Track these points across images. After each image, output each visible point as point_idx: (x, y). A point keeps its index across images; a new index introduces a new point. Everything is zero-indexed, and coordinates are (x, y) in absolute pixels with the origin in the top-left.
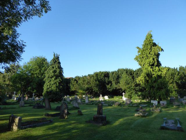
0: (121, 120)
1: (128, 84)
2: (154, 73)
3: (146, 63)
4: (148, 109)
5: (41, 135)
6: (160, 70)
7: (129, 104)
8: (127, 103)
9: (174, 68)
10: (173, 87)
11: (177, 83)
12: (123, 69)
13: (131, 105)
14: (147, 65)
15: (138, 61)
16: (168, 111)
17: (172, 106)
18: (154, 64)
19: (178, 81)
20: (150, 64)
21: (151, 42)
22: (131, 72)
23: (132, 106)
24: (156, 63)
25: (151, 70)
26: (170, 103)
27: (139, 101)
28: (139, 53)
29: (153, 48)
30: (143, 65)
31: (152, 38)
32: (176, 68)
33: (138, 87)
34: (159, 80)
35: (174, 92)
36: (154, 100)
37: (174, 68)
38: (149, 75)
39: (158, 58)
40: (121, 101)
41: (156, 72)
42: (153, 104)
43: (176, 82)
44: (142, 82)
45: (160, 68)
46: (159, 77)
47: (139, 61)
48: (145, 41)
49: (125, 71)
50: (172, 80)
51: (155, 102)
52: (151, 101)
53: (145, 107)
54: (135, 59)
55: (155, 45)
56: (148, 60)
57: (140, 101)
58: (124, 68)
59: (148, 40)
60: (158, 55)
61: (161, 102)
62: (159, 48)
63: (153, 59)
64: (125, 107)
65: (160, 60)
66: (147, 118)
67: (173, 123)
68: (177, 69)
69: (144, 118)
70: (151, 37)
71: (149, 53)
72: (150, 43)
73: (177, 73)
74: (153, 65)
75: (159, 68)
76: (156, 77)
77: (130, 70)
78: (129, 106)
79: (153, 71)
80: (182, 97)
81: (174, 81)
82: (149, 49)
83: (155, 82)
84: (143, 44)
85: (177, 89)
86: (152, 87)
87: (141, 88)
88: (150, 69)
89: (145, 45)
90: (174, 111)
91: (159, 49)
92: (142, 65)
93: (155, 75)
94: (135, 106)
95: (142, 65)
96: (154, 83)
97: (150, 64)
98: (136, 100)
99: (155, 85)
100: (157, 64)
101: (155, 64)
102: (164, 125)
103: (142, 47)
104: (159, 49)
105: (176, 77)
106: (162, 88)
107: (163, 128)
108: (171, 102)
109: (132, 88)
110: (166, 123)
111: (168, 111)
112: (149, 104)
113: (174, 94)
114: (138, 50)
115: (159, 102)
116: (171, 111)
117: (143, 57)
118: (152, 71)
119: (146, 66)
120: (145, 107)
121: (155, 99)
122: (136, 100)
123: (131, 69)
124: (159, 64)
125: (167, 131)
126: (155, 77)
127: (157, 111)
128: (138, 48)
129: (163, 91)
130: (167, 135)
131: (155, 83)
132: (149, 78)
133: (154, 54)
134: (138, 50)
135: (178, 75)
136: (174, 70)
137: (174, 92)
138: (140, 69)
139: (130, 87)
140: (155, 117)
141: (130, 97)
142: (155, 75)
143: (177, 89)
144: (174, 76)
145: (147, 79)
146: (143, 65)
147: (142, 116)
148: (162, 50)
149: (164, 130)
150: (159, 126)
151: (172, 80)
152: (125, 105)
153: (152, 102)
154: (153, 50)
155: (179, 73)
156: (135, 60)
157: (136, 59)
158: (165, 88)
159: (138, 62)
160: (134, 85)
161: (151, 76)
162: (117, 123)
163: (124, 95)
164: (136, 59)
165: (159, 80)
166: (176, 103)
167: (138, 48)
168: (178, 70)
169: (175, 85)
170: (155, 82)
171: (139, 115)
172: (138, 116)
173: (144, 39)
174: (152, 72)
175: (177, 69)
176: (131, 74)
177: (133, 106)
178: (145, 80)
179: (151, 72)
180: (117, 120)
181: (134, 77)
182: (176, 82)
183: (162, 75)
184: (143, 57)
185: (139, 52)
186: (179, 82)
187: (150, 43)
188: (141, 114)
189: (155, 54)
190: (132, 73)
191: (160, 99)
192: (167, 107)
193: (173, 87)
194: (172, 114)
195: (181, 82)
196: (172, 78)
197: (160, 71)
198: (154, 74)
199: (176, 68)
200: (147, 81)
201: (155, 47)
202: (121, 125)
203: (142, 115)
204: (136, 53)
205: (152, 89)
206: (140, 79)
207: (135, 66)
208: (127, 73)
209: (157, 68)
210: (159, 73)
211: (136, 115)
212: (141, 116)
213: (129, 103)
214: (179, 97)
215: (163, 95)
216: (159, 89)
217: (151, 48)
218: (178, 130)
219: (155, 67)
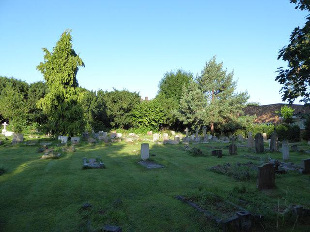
0: (24, 165)
1: (18, 108)
2: (68, 96)
3: (58, 78)
4: (56, 149)
5: (132, 156)
6: (76, 92)
7: (20, 142)
8: (14, 141)
9: (92, 91)
10: (88, 116)
11: (93, 113)
12: (5, 78)
13: (25, 144)
14: (59, 82)
15: (43, 72)
16: (83, 150)
17: (87, 144)
18: (69, 82)
19: (94, 110)
20: (62, 81)
21: (69, 48)
22: (22, 87)
23: (27, 146)
24: (72, 81)
25: (64, 90)
26: (84, 139)
27: (37, 137)
28: (47, 60)
29: (71, 57)
30: (52, 82)
31: (71, 42)
32: (93, 91)
33: (33, 114)
34: (74, 108)
35: (88, 125)
36: (62, 136)
37: (92, 91)
38: (59, 98)
39: (76, 75)
40: (3, 138)
41: (70, 95)
42: (60, 141)
43: (92, 111)
44: (47, 108)
45: (77, 90)
46: (74, 102)
47: (46, 74)
48: (59, 42)
49: (11, 84)
50: (87, 107)
51: (63, 139)
52: (58, 137)
53: (51, 145)
54: (37, 67)
55: (73, 53)
56: (60, 75)
57: (38, 138)
58: (9, 76)
59: (65, 43)
60: (76, 70)
61: (73, 138)
62: (79, 60)
63: (69, 75)
64: (13, 147)
65: (77, 77)
66: (60, 159)
67: (94, 162)
68: (95, 92)
69: (56, 160)
70: (70, 39)
71: (64, 65)
72: (67, 48)
73: (94, 99)
74: (67, 84)
75: (75, 89)
76: (69, 102)
77: (20, 81)
78: (21, 146)
79: (66, 92)
80: (96, 132)
81: (89, 109)
82: (64, 58)
83: (67, 109)
84: (55, 46)
85: (91, 120)
86: (62, 116)
87: (38, 115)
88: (61, 88)
89: (59, 50)
90: (90, 150)
91: (79, 62)
92: (50, 81)
93: (68, 100)
94: (31, 146)
95: (50, 81)
96: (66, 110)
97: (62, 81)
98: (32, 134)
99: (66, 113)
100: (74, 83)
101: (70, 83)
102: (86, 164)
103: (53, 52)
104: (79, 62)
105: (93, 104)
106: (76, 119)
107: (86, 168)
108: (84, 138)
109: (24, 116)
110: (87, 162)
111: (83, 150)
112: (54, 141)
113: (88, 127)
114: (45, 53)
115: (69, 139)
116: (87, 150)
117: (53, 69)
118: (65, 92)
119: (57, 83)
120: (51, 145)
121: (64, 134)
122: (30, 136)
123: (23, 80)
124: (75, 84)
125: (90, 170)
126: (68, 102)
127: (70, 150)
128: (45, 50)
129: (77, 123)
130: (92, 173)
131: (67, 111)
132: (59, 102)
133: (71, 68)
134: (45, 53)
135: (96, 101)
136: (92, 93)
137: (88, 125)
138: (39, 84)
139: (20, 114)
140: (71, 158)
141: (19, 130)
142: (68, 100)
143: (91, 120)
144: (90, 103)
145: (56, 102)
146: (52, 82)
147: (54, 158)
148: (83, 64)
149: (88, 170)
150: (81, 167)
151: (87, 107)
152: (11, 143)
153: (59, 138)
154: (70, 61)
155: (97, 99)
156: (38, 69)
157: (41, 68)
158: (80, 118)
159: (43, 74)
160: (28, 110)
161: (63, 101)
162: (21, 169)
163: (5, 127)
164: (41, 68)
165: (73, 107)
166: (92, 140)
167: (45, 50)
168: (96, 94)
169: (90, 114)
170: (67, 109)
171: (49, 157)
172: (48, 158)
173: (58, 39)
174: (64, 94)
175: (95, 92)
176: (22, 91)
177: (29, 144)
178: (52, 105)
179: (63, 93)
180: (17, 166)
181: (27, 95)
182: (92, 111)
183: (78, 101)
184: (53, 69)
185: (46, 57)
186: (96, 111)
187: (67, 48)
188: (52, 155)
189: (72, 68)
190: (25, 88)
191: (72, 135)
192: (80, 145)
193: (88, 116)
194: (89, 153)
195: (98, 112)
196: (87, 105)
197: (76, 94)
198: (67, 98)
199: (93, 91)
200: (56, 107)
201: (73, 57)
202: (27, 172)
203: (53, 156)
204: (41, 59)
205: (61, 119)
206: (44, 104)
207: (32, 76)
208: (14, 85)
209: (72, 89)
210: (75, 97)
211: (43, 157)
212: (53, 158)
213: (19, 140)
214: (93, 131)
215: (77, 128)
216: (72, 119)
217: (67, 57)
218: (101, 168)
219: (70, 87)
